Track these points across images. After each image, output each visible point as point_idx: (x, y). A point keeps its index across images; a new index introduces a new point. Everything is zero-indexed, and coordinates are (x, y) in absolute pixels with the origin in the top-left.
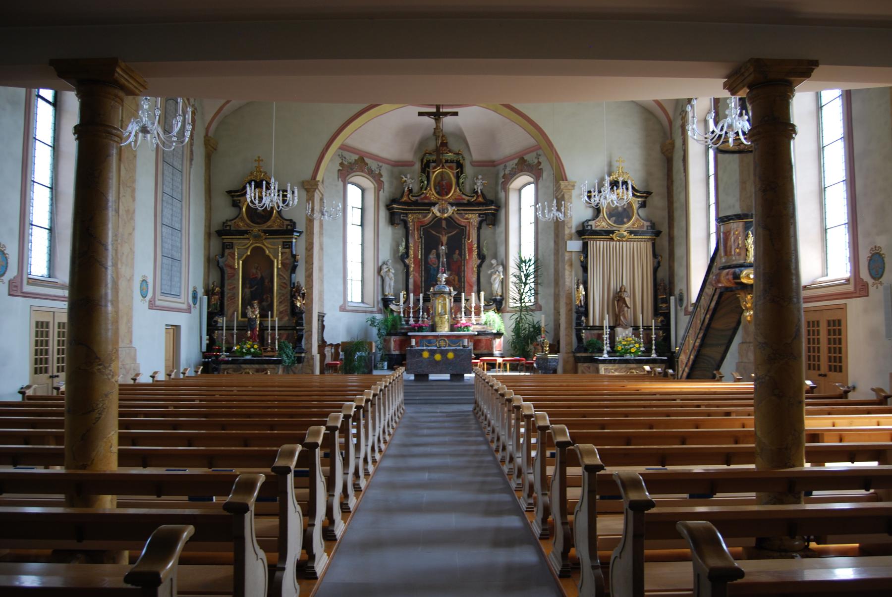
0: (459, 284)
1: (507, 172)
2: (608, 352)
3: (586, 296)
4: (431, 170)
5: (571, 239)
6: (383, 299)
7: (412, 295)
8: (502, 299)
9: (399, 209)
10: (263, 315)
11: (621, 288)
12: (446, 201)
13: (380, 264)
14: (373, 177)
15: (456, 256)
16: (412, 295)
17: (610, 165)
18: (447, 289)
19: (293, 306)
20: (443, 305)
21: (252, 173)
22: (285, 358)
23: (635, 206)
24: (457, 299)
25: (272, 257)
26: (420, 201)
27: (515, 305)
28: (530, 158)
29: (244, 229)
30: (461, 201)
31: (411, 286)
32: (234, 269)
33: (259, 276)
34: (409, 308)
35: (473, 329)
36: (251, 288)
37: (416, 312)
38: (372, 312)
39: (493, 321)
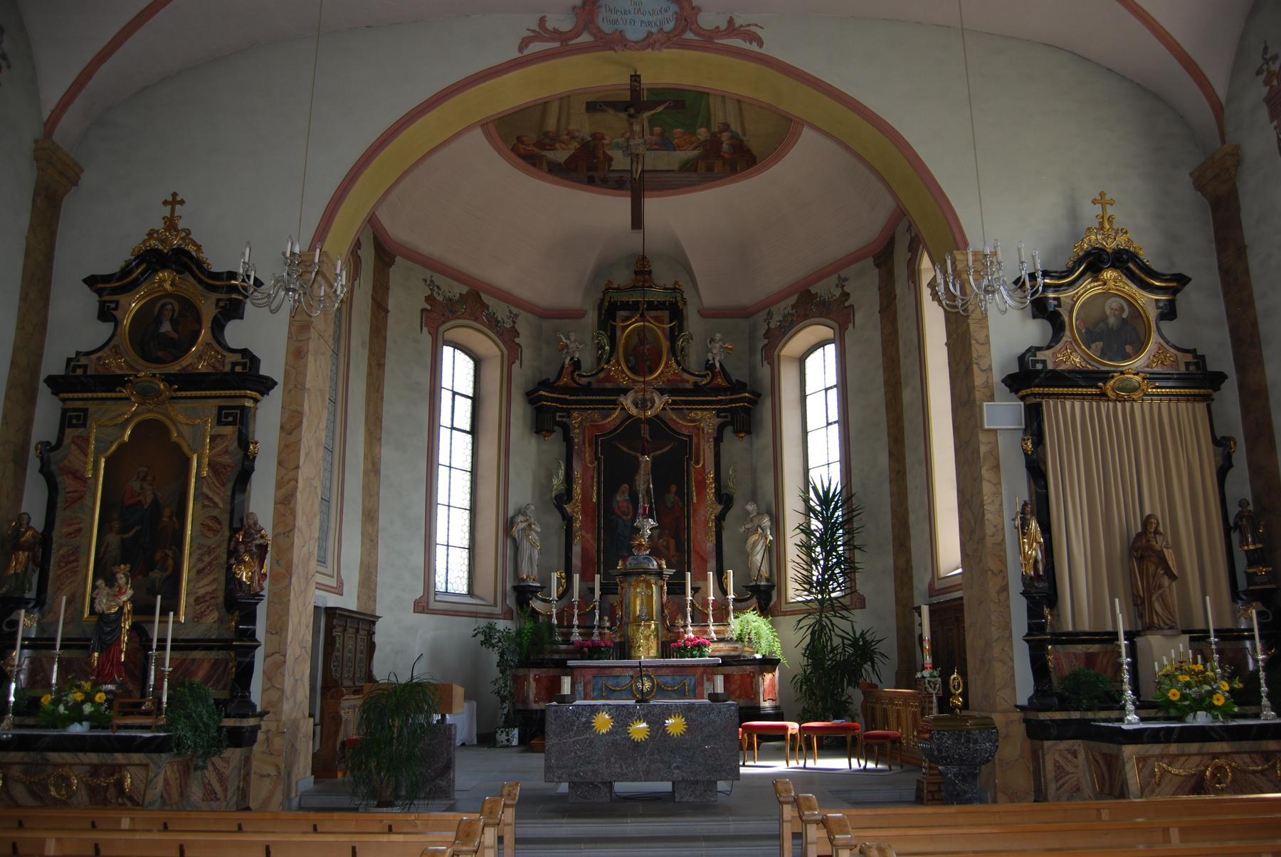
0: (678, 548)
1: (773, 325)
2: (1140, 706)
3: (1048, 549)
5: (991, 398)
6: (515, 588)
7: (576, 577)
8: (770, 588)
9: (547, 402)
10: (143, 609)
11: (1146, 521)
12: (649, 383)
13: (511, 513)
14: (500, 335)
15: (671, 497)
16: (576, 577)
18: (654, 565)
19: (232, 581)
20: (645, 598)
22: (183, 730)
23: (1152, 314)
24: (676, 588)
25: (186, 449)
26: (595, 386)
27: (811, 597)
28: (820, 289)
29: (119, 372)
30: (681, 385)
31: (576, 561)
32: (84, 480)
33: (149, 499)
34: (571, 606)
35: (715, 650)
36: (122, 531)
37: (586, 617)
38: (490, 616)
39: (755, 629)
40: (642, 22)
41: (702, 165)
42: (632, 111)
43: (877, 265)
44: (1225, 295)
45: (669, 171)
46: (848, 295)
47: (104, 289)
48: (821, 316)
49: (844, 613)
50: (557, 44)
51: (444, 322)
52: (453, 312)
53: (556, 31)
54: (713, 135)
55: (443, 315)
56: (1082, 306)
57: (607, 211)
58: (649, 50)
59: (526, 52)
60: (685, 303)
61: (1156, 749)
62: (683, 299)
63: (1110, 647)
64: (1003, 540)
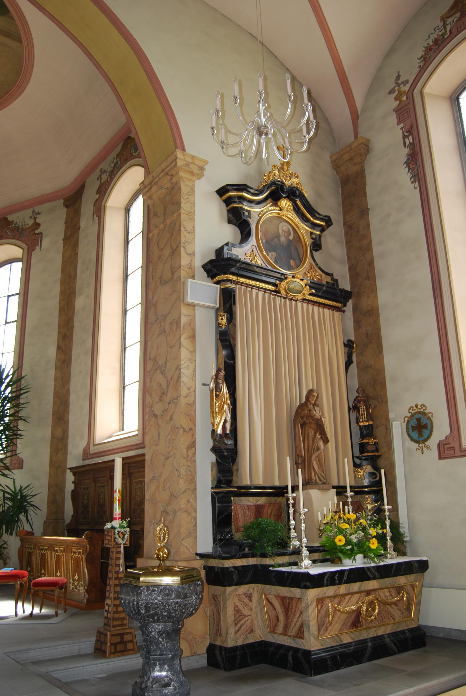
5: (193, 277)
23: (308, 241)
43: (66, 206)
44: (347, 243)
46: (38, 225)
48: (14, 238)
49: (6, 472)
61: (330, 591)
63: (280, 499)
64: (194, 401)
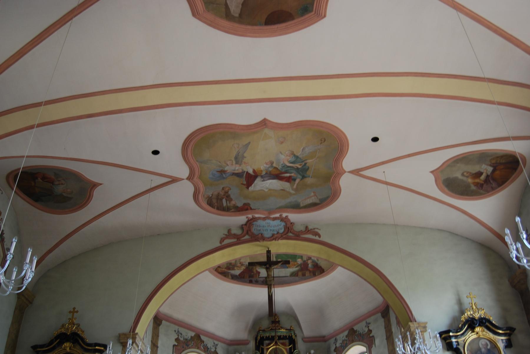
1: (338, 345)
4: (265, 348)
17: (460, 302)
21: (63, 326)
23: (501, 345)
28: (360, 328)
40: (270, 230)
41: (300, 274)
42: (268, 266)
45: (285, 277)
47: (40, 351)
48: (362, 341)
50: (235, 240)
51: (183, 351)
52: (188, 346)
53: (234, 234)
54: (304, 261)
55: (183, 347)
56: (469, 344)
57: (258, 295)
58: (274, 241)
59: (223, 244)
60: (296, 336)
62: (295, 334)
